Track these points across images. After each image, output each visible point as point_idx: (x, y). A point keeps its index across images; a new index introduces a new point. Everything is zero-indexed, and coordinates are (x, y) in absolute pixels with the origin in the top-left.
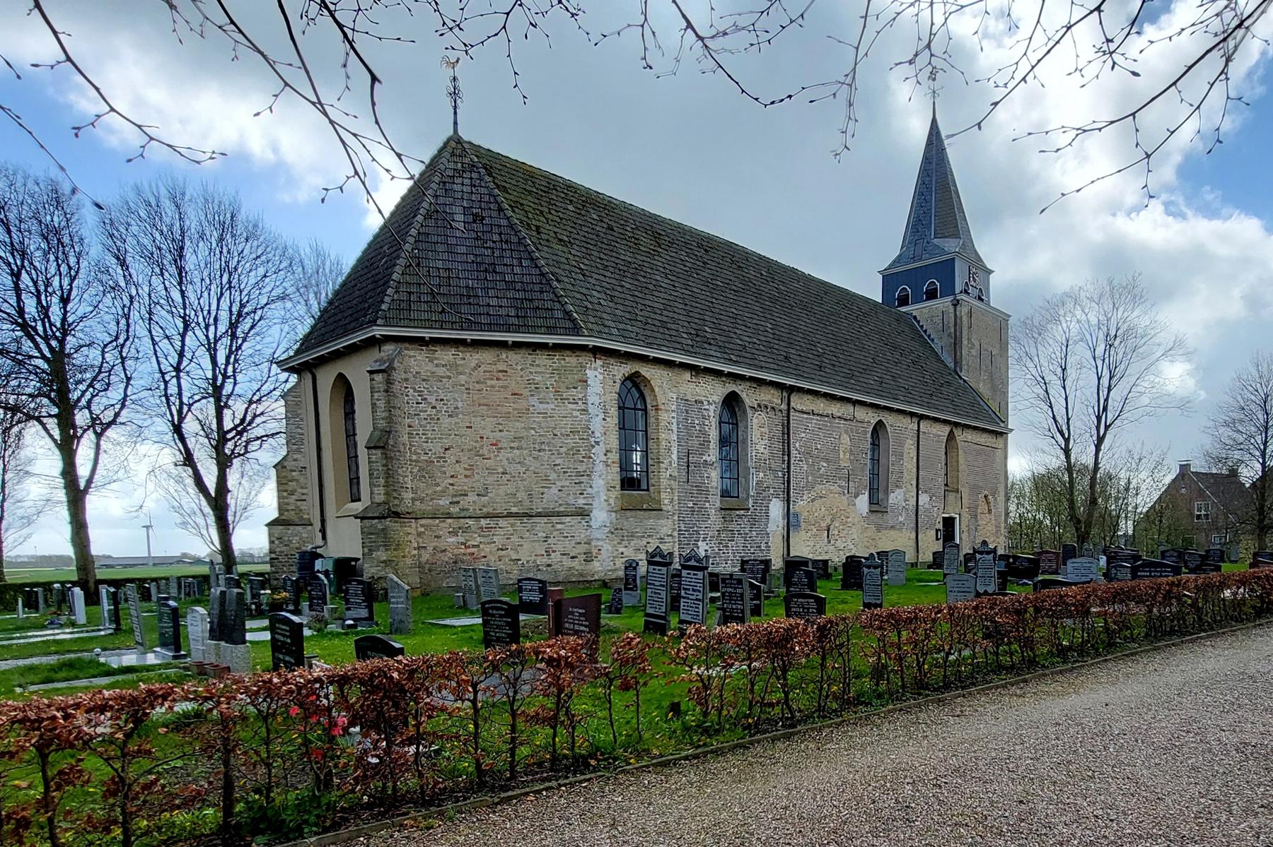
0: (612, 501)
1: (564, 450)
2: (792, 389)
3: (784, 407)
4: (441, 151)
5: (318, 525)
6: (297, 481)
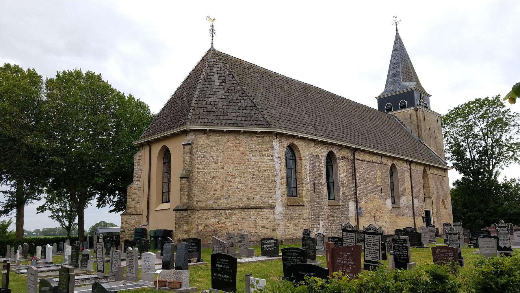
0: (283, 201)
1: (263, 177)
2: (356, 150)
3: (352, 158)
4: (206, 55)
5: (145, 214)
6: (137, 194)
